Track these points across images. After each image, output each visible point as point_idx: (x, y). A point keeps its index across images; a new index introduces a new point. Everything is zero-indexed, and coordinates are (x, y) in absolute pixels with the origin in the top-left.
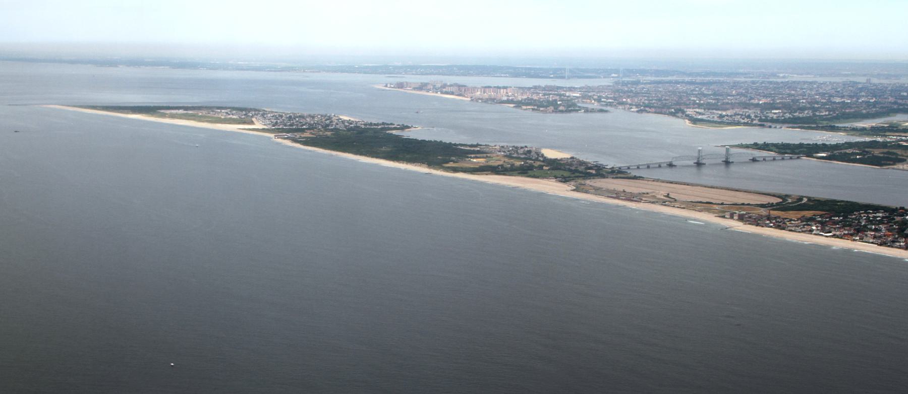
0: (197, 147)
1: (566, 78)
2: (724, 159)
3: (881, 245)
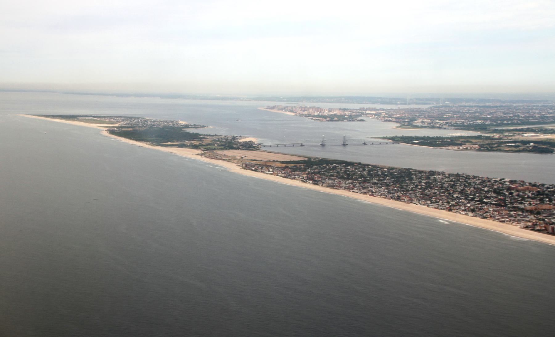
0: (46, 133)
2: (343, 143)
3: (285, 177)
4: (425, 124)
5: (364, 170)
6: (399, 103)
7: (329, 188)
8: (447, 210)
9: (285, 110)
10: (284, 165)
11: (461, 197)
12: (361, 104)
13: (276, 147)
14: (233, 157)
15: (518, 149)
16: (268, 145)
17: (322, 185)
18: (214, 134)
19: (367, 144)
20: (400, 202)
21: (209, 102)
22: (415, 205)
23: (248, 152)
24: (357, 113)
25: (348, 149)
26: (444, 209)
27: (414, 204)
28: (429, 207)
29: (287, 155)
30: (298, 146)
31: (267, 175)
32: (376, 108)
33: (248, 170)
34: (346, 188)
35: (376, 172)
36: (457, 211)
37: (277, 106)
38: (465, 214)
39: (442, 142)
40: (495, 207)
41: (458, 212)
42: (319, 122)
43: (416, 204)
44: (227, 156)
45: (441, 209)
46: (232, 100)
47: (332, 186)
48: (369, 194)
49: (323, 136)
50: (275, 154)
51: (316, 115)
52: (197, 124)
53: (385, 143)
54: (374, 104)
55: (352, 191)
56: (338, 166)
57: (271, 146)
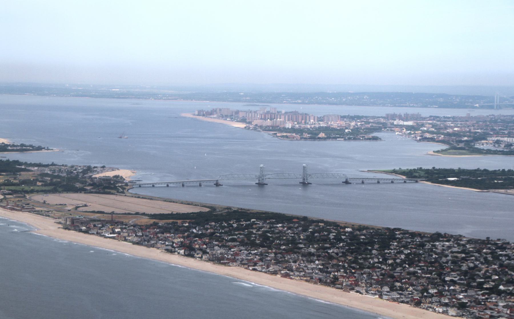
2: (301, 181)
3: (138, 243)
4: (499, 146)
5: (305, 230)
6: (477, 105)
7: (212, 263)
8: (413, 304)
9: (232, 118)
10: (152, 221)
16: (148, 184)
18: (61, 165)
19: (350, 183)
20: (334, 290)
22: (358, 294)
24: (374, 125)
25: (312, 192)
26: (407, 303)
27: (357, 292)
28: (382, 298)
29: (174, 202)
33: (73, 230)
34: (243, 262)
35: (326, 233)
36: (430, 305)
37: (218, 110)
38: (444, 312)
39: (505, 180)
42: (287, 141)
43: (361, 293)
44: (49, 204)
45: (402, 302)
47: (218, 260)
48: (281, 274)
49: (262, 165)
51: (288, 128)
53: (388, 181)
55: (251, 268)
56: (258, 223)
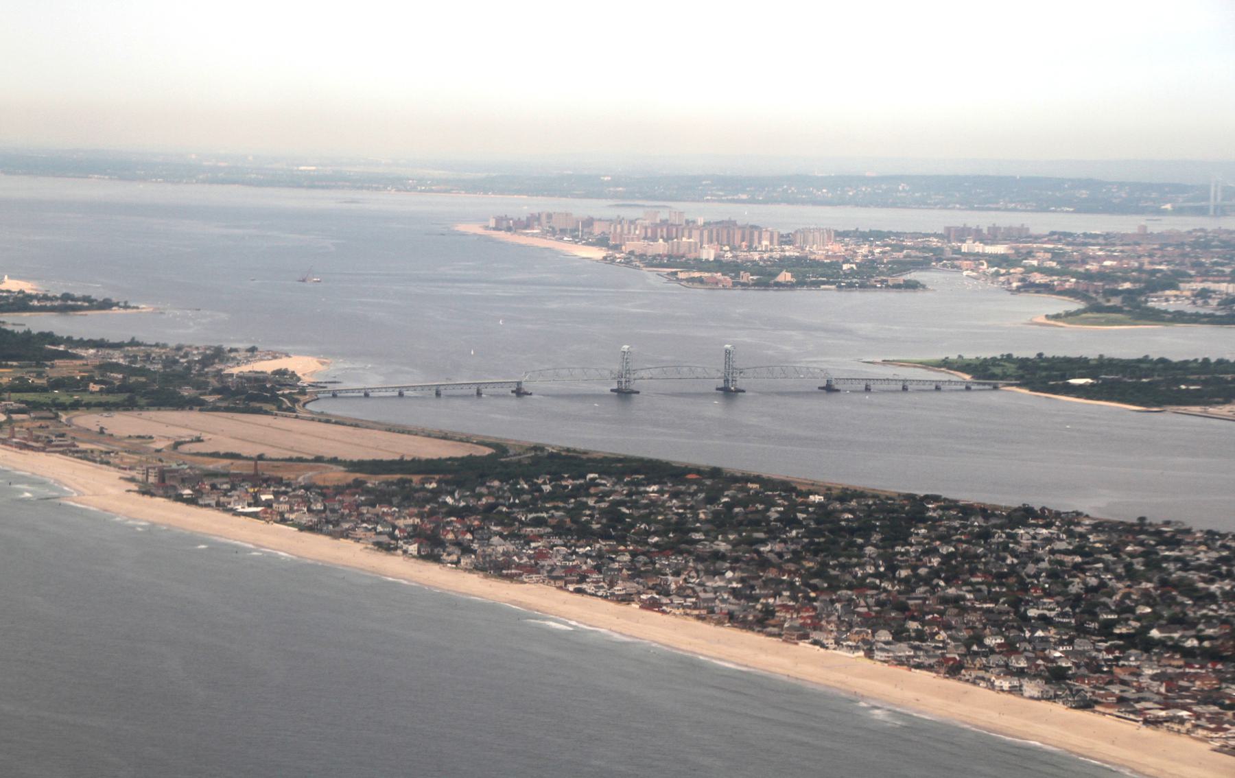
1: (1211, 212)
2: (721, 384)
3: (311, 529)
6: (1168, 206)
11: (1057, 619)
12: (984, 213)
13: (961, 390)
14: (138, 441)
15: (172, 475)
16: (353, 390)
17: (457, 563)
19: (838, 391)
21: (218, 195)
22: (817, 647)
23: (232, 418)
25: (747, 413)
26: (930, 668)
27: (815, 643)
28: (871, 658)
29: (409, 433)
30: (504, 396)
31: (236, 518)
32: (1028, 229)
33: (161, 496)
34: (555, 574)
38: (1012, 690)
40: (1181, 663)
41: (983, 679)
42: (701, 291)
43: (823, 646)
44: (112, 435)
46: (361, 188)
49: (626, 347)
50: (358, 431)
51: (707, 261)
52: (78, 294)
54: (1046, 210)
56: (603, 482)
57: (366, 395)
